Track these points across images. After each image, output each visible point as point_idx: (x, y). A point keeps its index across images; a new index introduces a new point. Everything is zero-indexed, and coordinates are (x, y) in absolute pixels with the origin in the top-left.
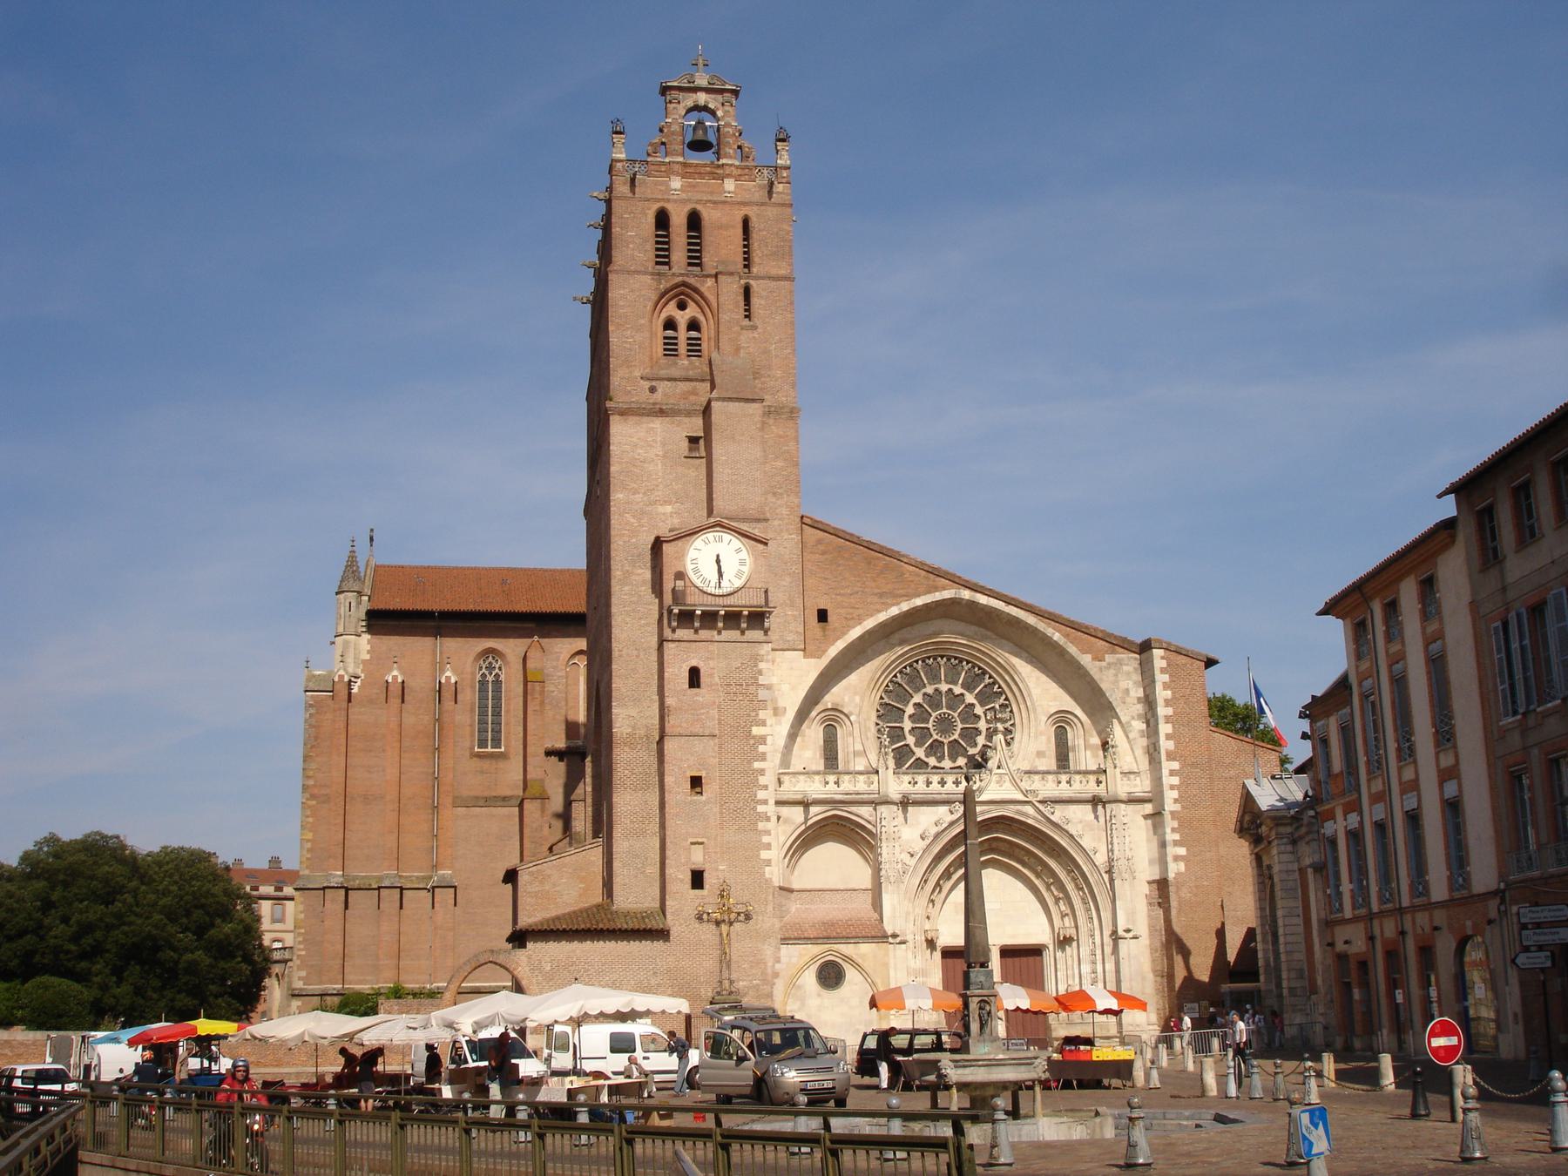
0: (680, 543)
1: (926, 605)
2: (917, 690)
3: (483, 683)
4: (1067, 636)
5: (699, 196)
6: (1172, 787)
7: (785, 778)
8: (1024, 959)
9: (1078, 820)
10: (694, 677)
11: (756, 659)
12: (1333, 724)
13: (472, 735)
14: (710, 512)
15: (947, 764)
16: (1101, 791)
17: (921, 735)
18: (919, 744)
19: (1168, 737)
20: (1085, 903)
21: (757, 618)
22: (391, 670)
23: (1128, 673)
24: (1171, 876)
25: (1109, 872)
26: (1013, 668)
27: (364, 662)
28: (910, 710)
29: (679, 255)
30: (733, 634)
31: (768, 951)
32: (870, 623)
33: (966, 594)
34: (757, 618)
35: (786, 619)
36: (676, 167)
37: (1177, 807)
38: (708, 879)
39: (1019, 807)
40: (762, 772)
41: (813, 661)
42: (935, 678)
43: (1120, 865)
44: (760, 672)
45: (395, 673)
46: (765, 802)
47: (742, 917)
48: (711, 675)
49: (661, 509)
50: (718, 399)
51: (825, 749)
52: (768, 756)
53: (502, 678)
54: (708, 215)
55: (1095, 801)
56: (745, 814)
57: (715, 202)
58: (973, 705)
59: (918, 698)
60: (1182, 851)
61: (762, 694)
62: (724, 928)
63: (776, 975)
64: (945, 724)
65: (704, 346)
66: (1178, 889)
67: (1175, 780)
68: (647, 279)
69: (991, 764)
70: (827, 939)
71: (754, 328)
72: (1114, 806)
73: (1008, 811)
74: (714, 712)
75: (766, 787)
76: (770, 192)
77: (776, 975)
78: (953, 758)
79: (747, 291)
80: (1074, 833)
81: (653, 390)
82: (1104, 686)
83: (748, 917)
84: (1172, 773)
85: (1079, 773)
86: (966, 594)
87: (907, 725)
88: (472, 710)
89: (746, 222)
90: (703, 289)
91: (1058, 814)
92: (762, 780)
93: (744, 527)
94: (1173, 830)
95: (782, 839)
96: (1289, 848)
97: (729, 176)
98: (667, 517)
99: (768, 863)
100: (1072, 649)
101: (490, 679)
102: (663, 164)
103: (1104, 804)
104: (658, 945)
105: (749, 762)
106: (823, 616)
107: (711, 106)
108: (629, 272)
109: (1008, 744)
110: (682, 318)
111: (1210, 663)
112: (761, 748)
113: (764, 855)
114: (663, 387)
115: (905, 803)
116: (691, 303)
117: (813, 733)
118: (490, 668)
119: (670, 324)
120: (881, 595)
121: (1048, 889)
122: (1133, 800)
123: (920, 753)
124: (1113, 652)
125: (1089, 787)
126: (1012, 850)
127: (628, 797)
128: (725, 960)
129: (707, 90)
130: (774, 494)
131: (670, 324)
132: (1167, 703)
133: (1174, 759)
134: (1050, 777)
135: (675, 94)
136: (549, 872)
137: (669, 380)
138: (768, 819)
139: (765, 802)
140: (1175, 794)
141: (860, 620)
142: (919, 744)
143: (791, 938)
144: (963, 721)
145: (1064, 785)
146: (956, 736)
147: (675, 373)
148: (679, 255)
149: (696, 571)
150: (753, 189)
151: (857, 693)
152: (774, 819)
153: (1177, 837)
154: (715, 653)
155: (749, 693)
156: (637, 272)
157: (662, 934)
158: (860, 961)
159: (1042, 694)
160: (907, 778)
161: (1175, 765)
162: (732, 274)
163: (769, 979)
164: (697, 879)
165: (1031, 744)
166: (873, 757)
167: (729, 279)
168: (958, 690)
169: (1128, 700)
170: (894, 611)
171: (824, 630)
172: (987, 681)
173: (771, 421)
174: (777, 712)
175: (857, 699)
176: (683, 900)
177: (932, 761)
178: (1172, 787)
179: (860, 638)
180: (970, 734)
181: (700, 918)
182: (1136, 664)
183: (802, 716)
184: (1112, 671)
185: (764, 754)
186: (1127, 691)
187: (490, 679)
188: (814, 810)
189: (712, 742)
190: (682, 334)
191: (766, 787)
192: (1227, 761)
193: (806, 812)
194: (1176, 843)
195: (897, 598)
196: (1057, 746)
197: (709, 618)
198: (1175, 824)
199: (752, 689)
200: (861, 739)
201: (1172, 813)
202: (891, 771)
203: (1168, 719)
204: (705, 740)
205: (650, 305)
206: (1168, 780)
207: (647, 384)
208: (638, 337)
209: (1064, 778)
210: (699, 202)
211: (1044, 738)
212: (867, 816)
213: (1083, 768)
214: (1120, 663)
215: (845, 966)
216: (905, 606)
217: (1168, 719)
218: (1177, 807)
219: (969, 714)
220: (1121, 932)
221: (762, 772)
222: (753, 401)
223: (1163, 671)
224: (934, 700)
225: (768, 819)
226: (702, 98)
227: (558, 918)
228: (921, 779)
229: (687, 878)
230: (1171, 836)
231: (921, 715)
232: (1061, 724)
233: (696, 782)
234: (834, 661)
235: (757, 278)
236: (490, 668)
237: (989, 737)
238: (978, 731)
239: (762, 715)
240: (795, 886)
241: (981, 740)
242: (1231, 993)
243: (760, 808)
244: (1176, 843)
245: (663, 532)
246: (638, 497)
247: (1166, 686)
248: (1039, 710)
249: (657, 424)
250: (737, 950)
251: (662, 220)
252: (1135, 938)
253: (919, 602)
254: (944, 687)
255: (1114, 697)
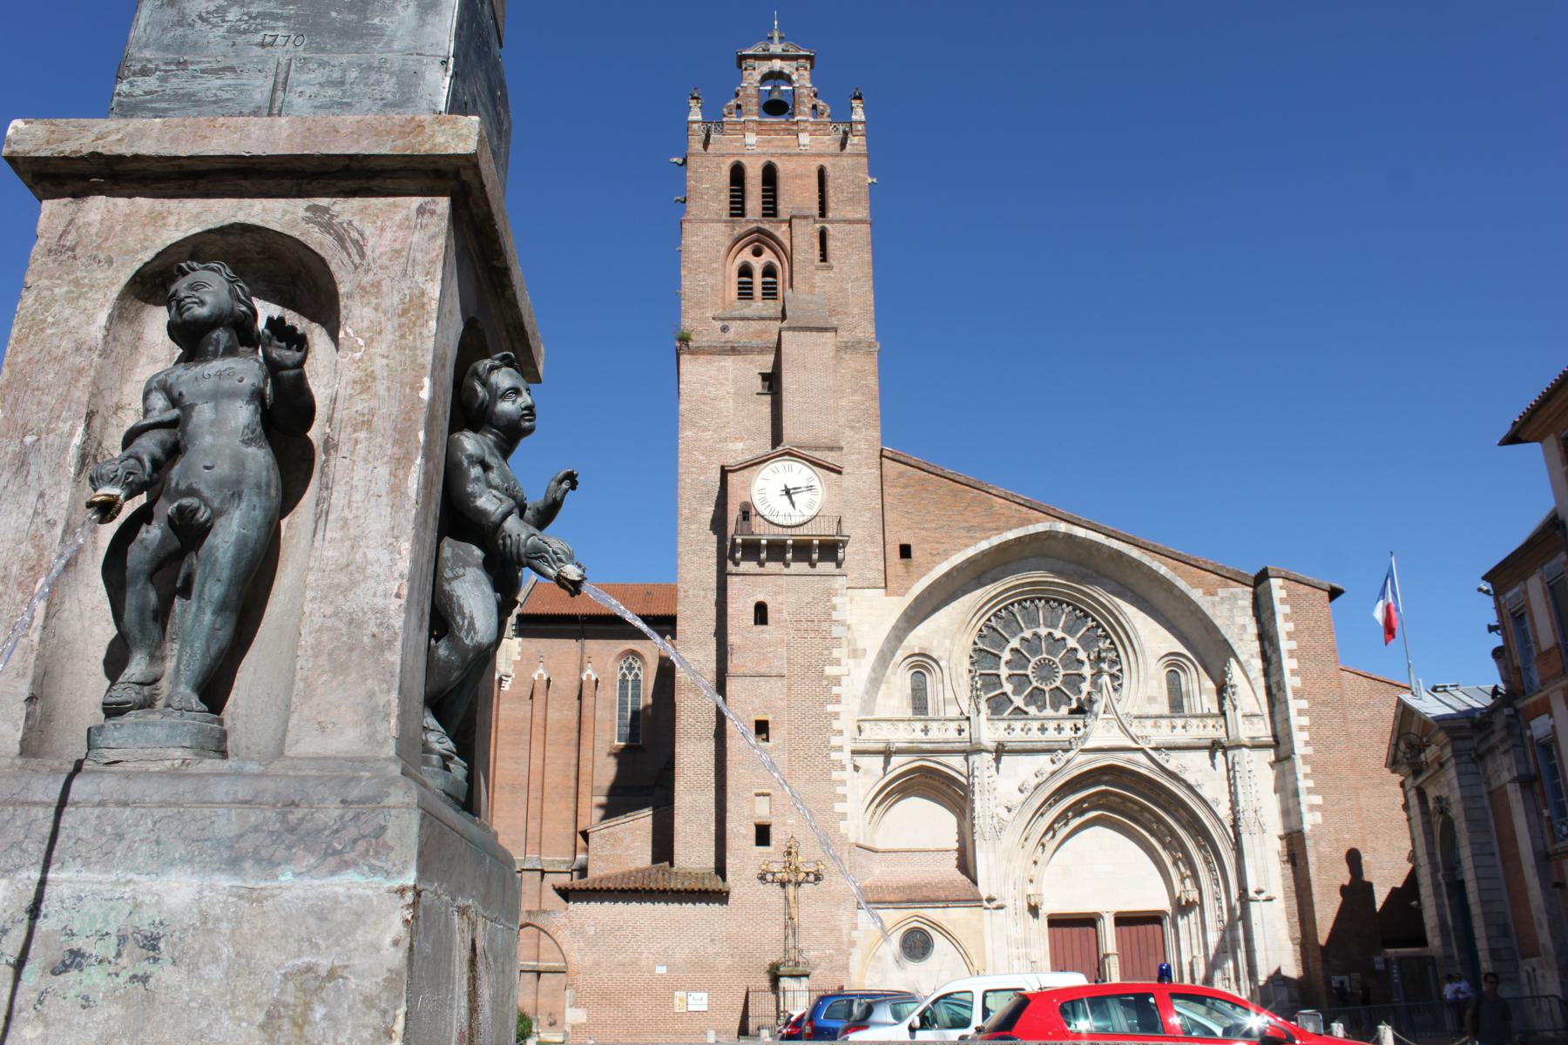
0: (745, 472)
1: (1019, 539)
2: (1014, 635)
3: (624, 681)
4: (1174, 569)
5: (773, 150)
6: (1301, 728)
7: (866, 726)
8: (1141, 928)
9: (1196, 768)
10: (761, 613)
11: (829, 593)
12: (1535, 589)
13: (612, 729)
14: (777, 438)
15: (1049, 712)
16: (1220, 734)
17: (1020, 681)
18: (1017, 692)
19: (1293, 673)
20: (1207, 862)
21: (830, 550)
22: (536, 668)
23: (1243, 608)
24: (1307, 827)
25: (1235, 826)
26: (1117, 607)
27: (515, 663)
28: (1006, 655)
29: (754, 202)
30: (803, 567)
31: (843, 916)
32: (958, 558)
33: (1062, 527)
34: (830, 550)
35: (860, 553)
36: (751, 125)
37: (1309, 751)
38: (776, 835)
39: (1130, 755)
40: (836, 715)
41: (895, 599)
42: (1033, 622)
43: (1246, 818)
44: (834, 608)
45: (541, 671)
46: (840, 749)
47: (812, 878)
48: (779, 611)
49: (731, 446)
50: (789, 329)
51: (914, 698)
52: (843, 699)
53: (641, 677)
54: (784, 167)
55: (1214, 747)
56: (816, 758)
57: (790, 155)
58: (1075, 650)
59: (1015, 643)
60: (1318, 800)
61: (836, 631)
62: (790, 888)
63: (853, 944)
64: (1046, 670)
65: (780, 288)
66: (1316, 843)
67: (1305, 721)
68: (721, 226)
69: (1098, 707)
70: (910, 902)
71: (830, 268)
72: (1236, 752)
73: (1118, 760)
74: (783, 651)
75: (840, 732)
76: (843, 145)
77: (853, 944)
78: (1056, 707)
79: (823, 236)
80: (1191, 781)
81: (724, 329)
82: (1218, 622)
83: (818, 878)
84: (1300, 713)
85: (1196, 717)
86: (1062, 527)
87: (1004, 672)
88: (612, 707)
89: (822, 173)
90: (777, 234)
91: (1173, 762)
92: (836, 725)
93: (817, 455)
94: (1306, 776)
95: (862, 792)
96: (1472, 767)
97: (803, 131)
98: (737, 451)
99: (843, 816)
100: (1181, 584)
101: (630, 678)
102: (736, 123)
103: (1225, 749)
104: (715, 908)
105: (822, 705)
106: (905, 551)
107: (786, 71)
108: (702, 221)
109: (1115, 690)
110: (757, 264)
111: (1334, 593)
112: (835, 690)
113: (839, 807)
114: (735, 326)
115: (1000, 751)
116: (767, 250)
117: (900, 680)
118: (630, 668)
119: (745, 271)
120: (969, 529)
121: (1175, 864)
122: (1257, 746)
123: (1019, 701)
124: (1227, 586)
125: (1213, 731)
126: (1122, 806)
127: (691, 747)
128: (790, 926)
129: (782, 58)
130: (852, 428)
131: (745, 271)
132: (1290, 636)
133: (1302, 697)
134: (1164, 723)
135: (750, 62)
136: (621, 834)
137: (742, 319)
138: (843, 768)
139: (840, 749)
140: (1305, 736)
141: (946, 555)
142: (1017, 692)
143: (875, 900)
144: (1065, 667)
145: (1179, 729)
146: (1058, 683)
147: (748, 312)
148: (754, 202)
149: (763, 501)
150: (829, 142)
151: (950, 633)
152: (850, 767)
153: (1310, 783)
154: (780, 586)
155: (821, 628)
156: (708, 221)
157: (721, 897)
158: (950, 928)
159: (1152, 638)
160: (1004, 725)
161: (1304, 704)
162: (806, 217)
163: (845, 948)
164: (763, 835)
165: (1143, 687)
166: (965, 704)
167: (804, 222)
168: (1058, 634)
169: (1246, 637)
170: (984, 545)
171: (907, 566)
172: (1090, 624)
173: (847, 357)
174: (855, 653)
175: (947, 643)
176: (744, 855)
177: (1032, 710)
178: (1301, 728)
179: (948, 575)
180: (1074, 680)
181: (762, 878)
182: (1249, 597)
183: (885, 657)
184: (1226, 606)
185: (838, 696)
186: (1244, 627)
187: (630, 678)
188: (896, 760)
189: (779, 683)
190: (758, 279)
191: (840, 732)
192: (1359, 701)
193: (887, 763)
194: (1310, 791)
195: (987, 532)
196: (1170, 691)
197: (777, 550)
198: (1308, 769)
199: (825, 625)
200: (954, 684)
201: (1303, 757)
202: (983, 716)
203: (1291, 653)
204: (772, 680)
205: (723, 250)
206: (1296, 721)
207: (719, 324)
208: (710, 280)
209: (1179, 722)
210: (773, 155)
211: (1155, 683)
212: (958, 767)
213: (1199, 712)
214: (1234, 597)
215: (933, 933)
216: (996, 540)
217: (1291, 653)
218: (1309, 751)
219: (1072, 660)
220: (1251, 894)
221: (836, 715)
222: (825, 330)
223: (1283, 601)
224: (1033, 644)
225: (843, 768)
226: (777, 65)
227: (609, 878)
228: (1018, 725)
229: (752, 833)
230: (1304, 784)
231: (1019, 658)
232: (1174, 666)
233: (762, 728)
234: (919, 600)
235: (832, 222)
236: (630, 668)
237: (1094, 684)
238: (1082, 677)
239: (836, 653)
240: (879, 847)
241: (1086, 687)
242: (1400, 959)
243: (834, 756)
244: (1310, 791)
245: (730, 461)
246: (708, 435)
247: (1287, 618)
248: (1148, 652)
249: (729, 362)
250: (803, 916)
251: (738, 174)
252: (1269, 899)
253: (1011, 535)
254: (1043, 631)
255: (1230, 634)
